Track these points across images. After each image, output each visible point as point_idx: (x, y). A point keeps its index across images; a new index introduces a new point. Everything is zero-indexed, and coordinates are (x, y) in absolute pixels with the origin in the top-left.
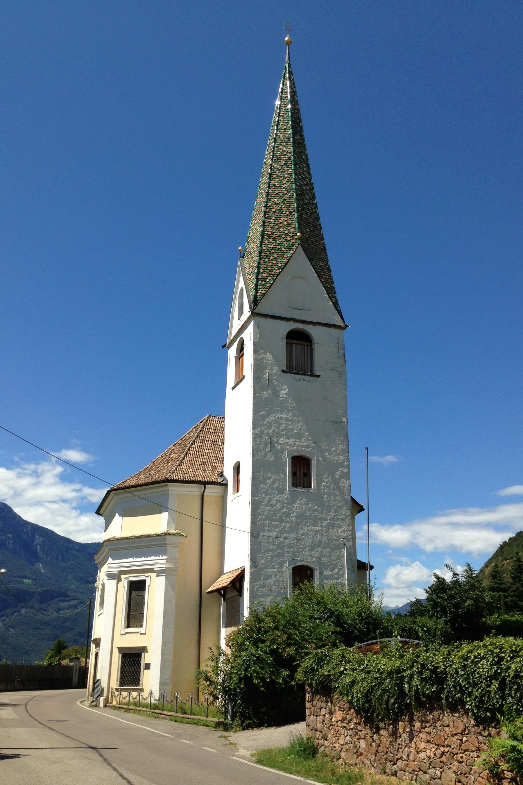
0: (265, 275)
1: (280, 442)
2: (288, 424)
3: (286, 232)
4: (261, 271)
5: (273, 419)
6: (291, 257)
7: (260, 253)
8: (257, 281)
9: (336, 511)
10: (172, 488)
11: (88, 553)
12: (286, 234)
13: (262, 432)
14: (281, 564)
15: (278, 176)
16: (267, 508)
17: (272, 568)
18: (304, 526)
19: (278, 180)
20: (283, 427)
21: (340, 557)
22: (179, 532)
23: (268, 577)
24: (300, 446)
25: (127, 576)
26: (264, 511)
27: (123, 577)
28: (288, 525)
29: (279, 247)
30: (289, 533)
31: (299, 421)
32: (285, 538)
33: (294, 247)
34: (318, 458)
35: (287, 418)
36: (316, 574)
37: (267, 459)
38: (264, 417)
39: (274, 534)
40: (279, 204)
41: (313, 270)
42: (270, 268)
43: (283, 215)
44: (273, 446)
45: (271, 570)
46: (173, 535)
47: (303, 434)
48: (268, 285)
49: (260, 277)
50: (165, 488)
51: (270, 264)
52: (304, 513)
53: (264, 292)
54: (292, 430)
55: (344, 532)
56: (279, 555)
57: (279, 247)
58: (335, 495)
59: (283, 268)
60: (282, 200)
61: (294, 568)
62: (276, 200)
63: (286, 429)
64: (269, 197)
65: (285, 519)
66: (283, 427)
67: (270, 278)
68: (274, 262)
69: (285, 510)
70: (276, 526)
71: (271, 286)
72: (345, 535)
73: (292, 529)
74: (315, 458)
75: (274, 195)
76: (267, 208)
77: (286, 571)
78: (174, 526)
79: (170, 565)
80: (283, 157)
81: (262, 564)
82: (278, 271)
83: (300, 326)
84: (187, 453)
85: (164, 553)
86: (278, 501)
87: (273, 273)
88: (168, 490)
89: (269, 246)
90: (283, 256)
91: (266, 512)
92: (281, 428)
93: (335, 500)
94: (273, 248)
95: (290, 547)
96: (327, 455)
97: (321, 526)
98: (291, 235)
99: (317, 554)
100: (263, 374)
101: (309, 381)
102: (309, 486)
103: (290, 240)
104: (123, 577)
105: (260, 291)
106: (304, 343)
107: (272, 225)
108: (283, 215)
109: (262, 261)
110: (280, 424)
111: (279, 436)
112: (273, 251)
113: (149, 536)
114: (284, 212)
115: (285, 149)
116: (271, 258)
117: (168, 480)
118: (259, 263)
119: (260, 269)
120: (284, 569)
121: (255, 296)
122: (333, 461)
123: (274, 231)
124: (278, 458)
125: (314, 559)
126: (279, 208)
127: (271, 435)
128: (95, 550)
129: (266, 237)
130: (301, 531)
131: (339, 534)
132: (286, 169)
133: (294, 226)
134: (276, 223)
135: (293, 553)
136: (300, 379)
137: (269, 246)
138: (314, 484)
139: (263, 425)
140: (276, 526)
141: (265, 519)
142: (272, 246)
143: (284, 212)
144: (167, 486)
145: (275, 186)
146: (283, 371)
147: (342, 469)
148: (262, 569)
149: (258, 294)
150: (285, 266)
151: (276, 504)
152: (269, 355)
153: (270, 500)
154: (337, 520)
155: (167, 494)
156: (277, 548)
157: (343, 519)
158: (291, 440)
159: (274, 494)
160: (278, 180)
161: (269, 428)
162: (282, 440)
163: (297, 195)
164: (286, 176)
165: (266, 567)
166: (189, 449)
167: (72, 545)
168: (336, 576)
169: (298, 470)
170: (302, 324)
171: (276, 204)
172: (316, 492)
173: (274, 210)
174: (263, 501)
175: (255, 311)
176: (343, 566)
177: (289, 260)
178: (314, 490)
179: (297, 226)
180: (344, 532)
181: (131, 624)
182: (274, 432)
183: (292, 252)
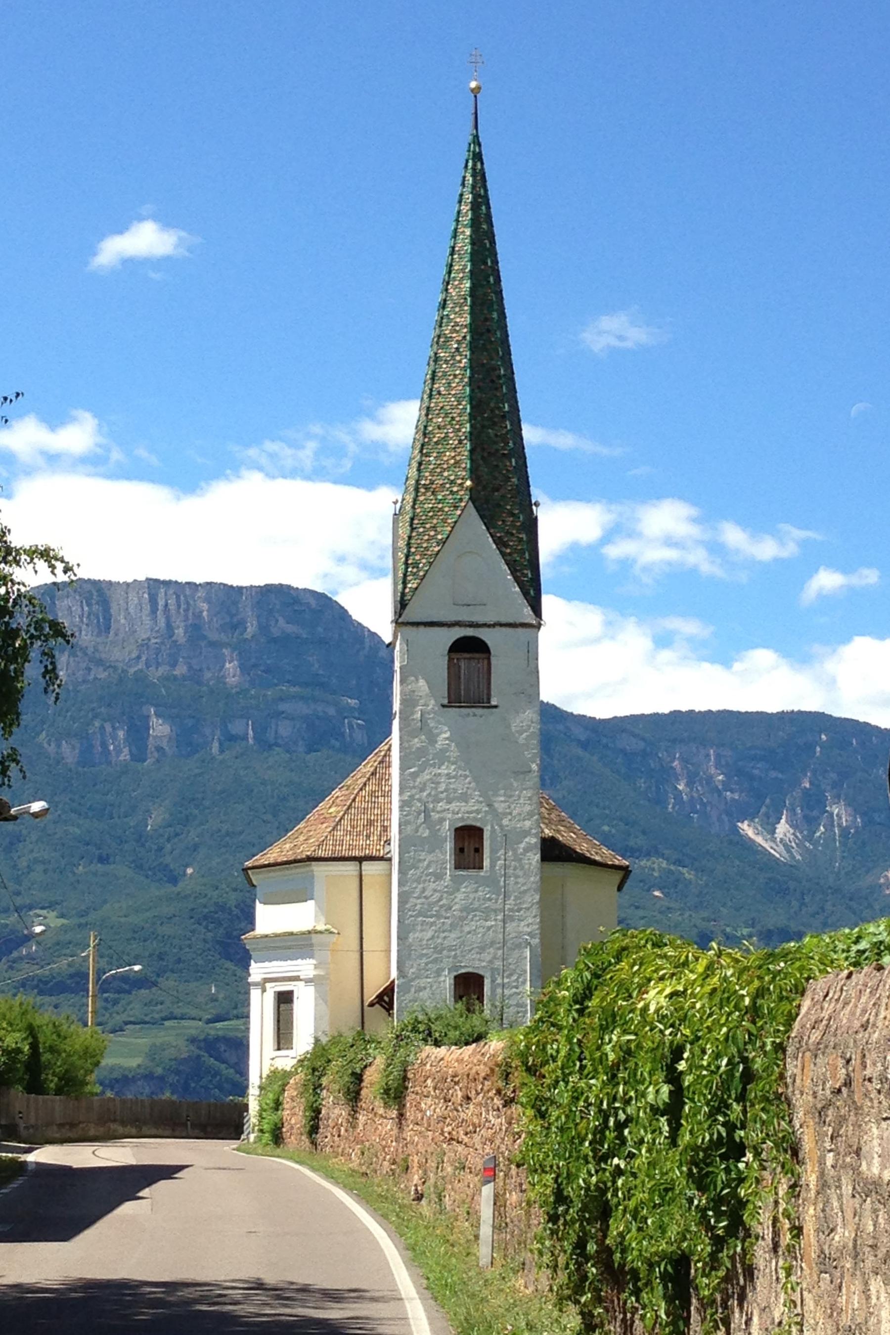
0: (418, 557)
1: (439, 809)
2: (450, 783)
3: (452, 478)
4: (413, 550)
5: (428, 777)
6: (456, 522)
7: (412, 519)
8: (407, 568)
9: (516, 898)
10: (319, 869)
11: (623, 751)
12: (452, 482)
13: (412, 797)
14: (438, 973)
15: (445, 374)
16: (419, 901)
17: (427, 977)
18: (472, 920)
19: (444, 381)
20: (442, 787)
21: (523, 958)
22: (329, 927)
23: (420, 989)
24: (468, 812)
25: (273, 984)
26: (416, 905)
27: (268, 985)
28: (449, 921)
29: (440, 506)
30: (450, 931)
31: (466, 777)
32: (445, 938)
33: (463, 504)
34: (492, 827)
35: (448, 774)
36: (487, 983)
37: (419, 834)
38: (415, 775)
39: (430, 934)
40: (445, 427)
41: (490, 539)
42: (425, 545)
43: (448, 447)
44: (427, 817)
45: (424, 980)
46: (321, 932)
47: (471, 795)
48: (421, 573)
49: (410, 562)
50: (308, 869)
51: (426, 537)
52: (471, 904)
53: (415, 586)
54: (455, 790)
55: (528, 925)
56: (435, 961)
57: (440, 506)
58: (517, 877)
59: (444, 543)
60: (449, 419)
61: (456, 977)
62: (440, 420)
63: (446, 790)
64: (430, 417)
65: (444, 914)
66: (442, 787)
67: (424, 561)
68: (432, 533)
69: (444, 901)
70: (432, 924)
71: (424, 576)
72: (529, 930)
73: (453, 926)
74: (489, 828)
75: (437, 412)
76: (425, 437)
77: (444, 981)
78: (323, 919)
79: (321, 973)
80: (454, 335)
81: (413, 973)
82: (437, 549)
83: (469, 632)
84: (349, 807)
85: (311, 957)
86: (435, 891)
87: (429, 553)
88: (312, 871)
89: (426, 506)
90: (444, 521)
91: (418, 907)
92: (439, 790)
93: (517, 883)
94: (432, 508)
95: (450, 950)
96: (505, 822)
97: (496, 920)
98: (459, 481)
99: (488, 958)
100: (413, 713)
101: (481, 716)
102: (481, 867)
103: (457, 491)
104: (268, 985)
105: (409, 585)
106: (477, 655)
107: (432, 467)
108: (448, 447)
109: (414, 534)
110: (439, 783)
111: (437, 800)
112: (431, 514)
113: (292, 934)
114: (451, 442)
115: (458, 320)
116: (428, 526)
117: (310, 859)
118: (410, 538)
119: (410, 548)
120: (442, 979)
121: (403, 594)
122: (515, 828)
123: (434, 478)
124: (434, 834)
125: (484, 964)
126: (443, 435)
127: (426, 800)
128: (643, 739)
129: (423, 490)
130: (467, 929)
131: (521, 929)
132: (458, 358)
133: (464, 465)
134: (438, 462)
135: (455, 957)
136: (468, 715)
137: (426, 506)
138: (486, 863)
139: (414, 787)
140: (432, 924)
141: (417, 916)
142: (430, 506)
143: (451, 442)
144: (310, 865)
145: (439, 393)
146: (443, 706)
147: (527, 840)
148: (413, 980)
149: (407, 590)
150: (447, 538)
151: (432, 895)
152: (422, 683)
153: (424, 890)
154: (519, 910)
155: (313, 877)
156: (434, 952)
157: (528, 909)
158: (453, 804)
159: (430, 881)
160: (444, 381)
161: (422, 790)
162: (441, 805)
163: (472, 408)
164: (458, 372)
165: (418, 977)
166: (354, 800)
167: (561, 727)
168: (514, 984)
169: (466, 844)
170: (472, 629)
171: (439, 428)
172: (488, 874)
173: (435, 440)
174: (413, 892)
175: (400, 620)
176: (525, 972)
177: (453, 528)
178: (486, 871)
179: (468, 466)
180: (528, 925)
181: (282, 1046)
182: (429, 795)
183: (459, 512)
